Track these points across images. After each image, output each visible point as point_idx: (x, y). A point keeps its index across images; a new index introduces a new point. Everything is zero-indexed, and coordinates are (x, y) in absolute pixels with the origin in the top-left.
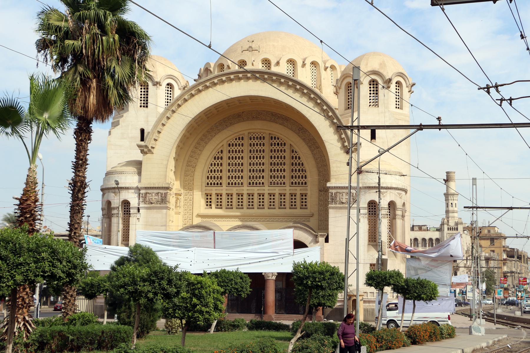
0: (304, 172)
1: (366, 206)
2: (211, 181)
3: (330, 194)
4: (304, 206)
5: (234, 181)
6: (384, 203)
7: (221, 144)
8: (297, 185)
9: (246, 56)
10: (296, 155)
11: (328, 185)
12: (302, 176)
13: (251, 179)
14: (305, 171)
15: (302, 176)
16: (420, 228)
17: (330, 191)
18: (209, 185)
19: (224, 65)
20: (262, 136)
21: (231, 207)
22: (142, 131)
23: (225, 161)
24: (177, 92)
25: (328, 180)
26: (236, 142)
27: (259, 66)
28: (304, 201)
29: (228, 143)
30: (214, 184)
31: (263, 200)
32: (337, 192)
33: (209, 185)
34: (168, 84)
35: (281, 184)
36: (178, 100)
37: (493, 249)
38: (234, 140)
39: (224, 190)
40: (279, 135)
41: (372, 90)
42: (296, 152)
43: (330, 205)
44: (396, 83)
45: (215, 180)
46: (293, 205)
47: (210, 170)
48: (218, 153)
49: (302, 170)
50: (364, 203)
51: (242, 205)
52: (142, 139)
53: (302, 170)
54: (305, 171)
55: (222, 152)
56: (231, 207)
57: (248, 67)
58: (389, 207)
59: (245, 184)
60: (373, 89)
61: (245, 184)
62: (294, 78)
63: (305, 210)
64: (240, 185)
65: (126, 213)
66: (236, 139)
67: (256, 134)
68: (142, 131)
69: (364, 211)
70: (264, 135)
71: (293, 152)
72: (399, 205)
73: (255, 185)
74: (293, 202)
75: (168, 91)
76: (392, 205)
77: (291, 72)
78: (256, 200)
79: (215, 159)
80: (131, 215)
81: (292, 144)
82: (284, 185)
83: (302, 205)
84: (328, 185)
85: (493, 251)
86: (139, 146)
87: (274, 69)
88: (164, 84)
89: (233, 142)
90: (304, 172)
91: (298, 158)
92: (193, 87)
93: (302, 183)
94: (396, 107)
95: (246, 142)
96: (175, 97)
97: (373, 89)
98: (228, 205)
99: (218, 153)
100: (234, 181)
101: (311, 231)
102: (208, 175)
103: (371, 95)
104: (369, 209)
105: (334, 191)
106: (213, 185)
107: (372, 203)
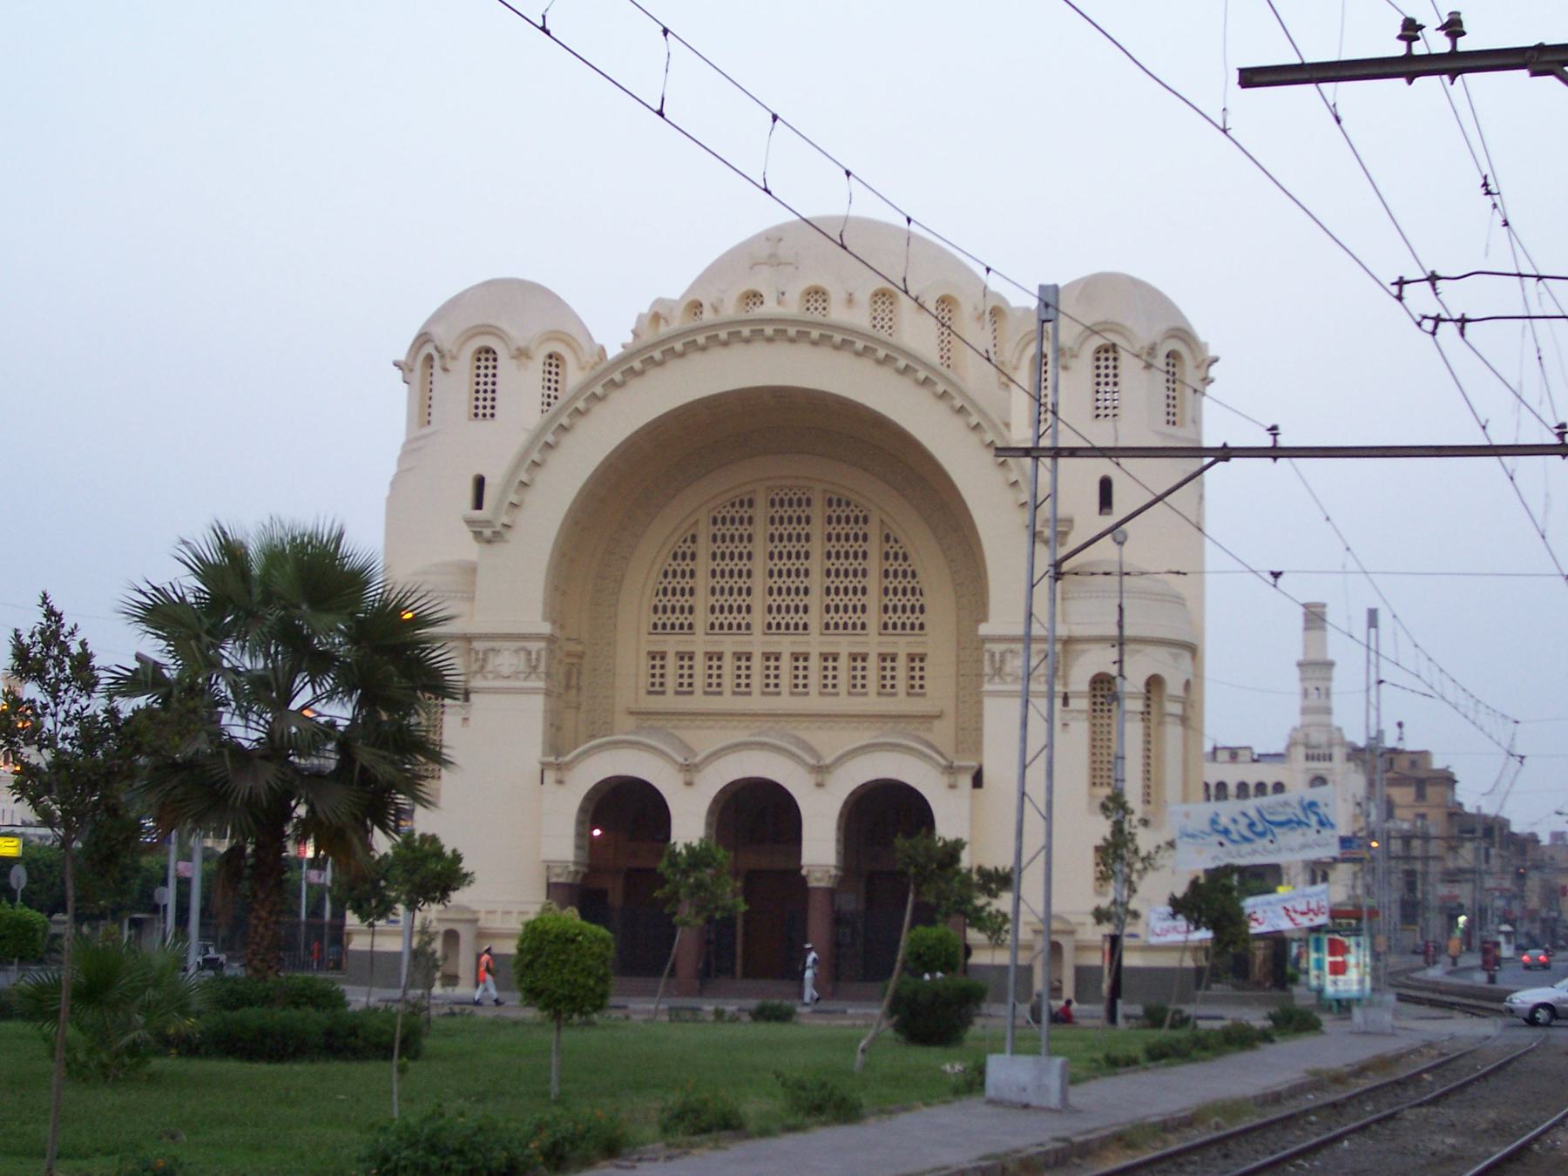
0: (918, 596)
1: (1084, 687)
2: (779, 618)
3: (987, 656)
4: (916, 687)
5: (725, 619)
6: (1134, 682)
7: (692, 520)
8: (899, 631)
9: (762, 282)
10: (896, 548)
11: (984, 629)
12: (913, 608)
13: (775, 613)
14: (921, 594)
15: (913, 608)
16: (1234, 754)
17: (988, 646)
18: (659, 630)
19: (701, 305)
20: (804, 498)
21: (747, 690)
22: (480, 483)
23: (703, 565)
24: (573, 377)
25: (983, 617)
26: (733, 512)
27: (793, 307)
28: (917, 673)
29: (712, 515)
30: (845, 626)
31: (662, 671)
32: (1006, 651)
33: (774, 630)
34: (550, 356)
35: (913, 627)
36: (575, 398)
37: (1422, 810)
38: (729, 508)
39: (757, 643)
40: (853, 497)
41: (485, 371)
42: (896, 541)
43: (987, 687)
44: (1168, 356)
45: (676, 615)
46: (686, 685)
47: (661, 587)
48: (685, 541)
49: (913, 589)
50: (1079, 678)
51: (805, 686)
52: (478, 505)
53: (913, 589)
54: (921, 594)
55: (694, 539)
56: (747, 690)
57: (770, 308)
58: (1148, 691)
59: (815, 627)
60: (490, 368)
61: (815, 627)
62: (890, 339)
63: (746, 698)
64: (743, 630)
65: (1098, 707)
66: (733, 505)
67: (795, 490)
68: (480, 483)
69: (1081, 704)
70: (808, 494)
71: (887, 538)
72: (1174, 686)
73: (783, 630)
74: (714, 677)
75: (550, 373)
76: (1154, 684)
77: (882, 323)
78: (902, 673)
79: (675, 557)
80: (446, 709)
81: (884, 517)
82: (748, 632)
83: (913, 687)
84: (984, 629)
85: (1423, 816)
86: (470, 522)
87: (838, 313)
88: (540, 357)
89: (724, 512)
90: (918, 596)
91: (901, 556)
92: (621, 360)
93: (681, 627)
94: (1168, 422)
95: (761, 512)
96: (568, 389)
97: (490, 368)
98: (653, 684)
99: (685, 541)
100: (725, 619)
101: (934, 755)
102: (655, 601)
103: (492, 387)
104: (1095, 696)
105: (997, 648)
106: (726, 630)
107: (1102, 682)
